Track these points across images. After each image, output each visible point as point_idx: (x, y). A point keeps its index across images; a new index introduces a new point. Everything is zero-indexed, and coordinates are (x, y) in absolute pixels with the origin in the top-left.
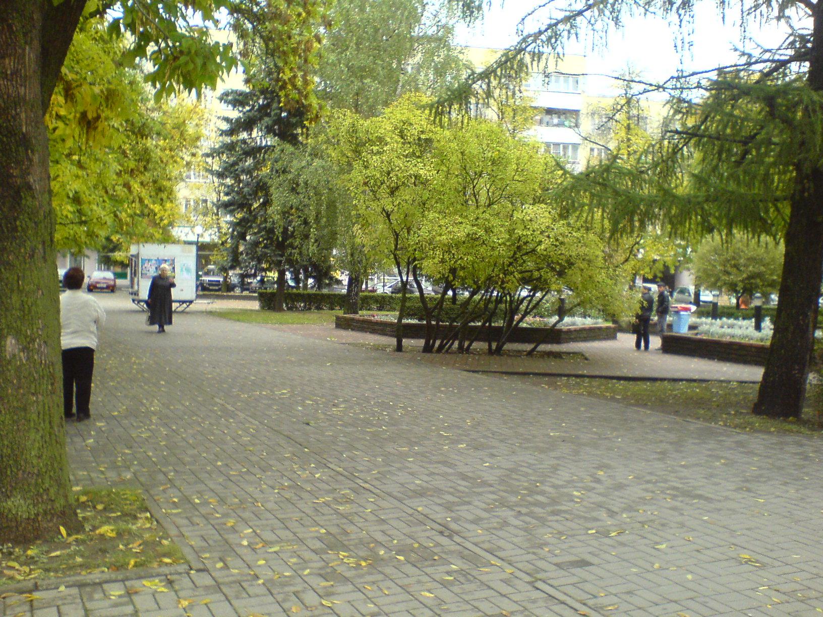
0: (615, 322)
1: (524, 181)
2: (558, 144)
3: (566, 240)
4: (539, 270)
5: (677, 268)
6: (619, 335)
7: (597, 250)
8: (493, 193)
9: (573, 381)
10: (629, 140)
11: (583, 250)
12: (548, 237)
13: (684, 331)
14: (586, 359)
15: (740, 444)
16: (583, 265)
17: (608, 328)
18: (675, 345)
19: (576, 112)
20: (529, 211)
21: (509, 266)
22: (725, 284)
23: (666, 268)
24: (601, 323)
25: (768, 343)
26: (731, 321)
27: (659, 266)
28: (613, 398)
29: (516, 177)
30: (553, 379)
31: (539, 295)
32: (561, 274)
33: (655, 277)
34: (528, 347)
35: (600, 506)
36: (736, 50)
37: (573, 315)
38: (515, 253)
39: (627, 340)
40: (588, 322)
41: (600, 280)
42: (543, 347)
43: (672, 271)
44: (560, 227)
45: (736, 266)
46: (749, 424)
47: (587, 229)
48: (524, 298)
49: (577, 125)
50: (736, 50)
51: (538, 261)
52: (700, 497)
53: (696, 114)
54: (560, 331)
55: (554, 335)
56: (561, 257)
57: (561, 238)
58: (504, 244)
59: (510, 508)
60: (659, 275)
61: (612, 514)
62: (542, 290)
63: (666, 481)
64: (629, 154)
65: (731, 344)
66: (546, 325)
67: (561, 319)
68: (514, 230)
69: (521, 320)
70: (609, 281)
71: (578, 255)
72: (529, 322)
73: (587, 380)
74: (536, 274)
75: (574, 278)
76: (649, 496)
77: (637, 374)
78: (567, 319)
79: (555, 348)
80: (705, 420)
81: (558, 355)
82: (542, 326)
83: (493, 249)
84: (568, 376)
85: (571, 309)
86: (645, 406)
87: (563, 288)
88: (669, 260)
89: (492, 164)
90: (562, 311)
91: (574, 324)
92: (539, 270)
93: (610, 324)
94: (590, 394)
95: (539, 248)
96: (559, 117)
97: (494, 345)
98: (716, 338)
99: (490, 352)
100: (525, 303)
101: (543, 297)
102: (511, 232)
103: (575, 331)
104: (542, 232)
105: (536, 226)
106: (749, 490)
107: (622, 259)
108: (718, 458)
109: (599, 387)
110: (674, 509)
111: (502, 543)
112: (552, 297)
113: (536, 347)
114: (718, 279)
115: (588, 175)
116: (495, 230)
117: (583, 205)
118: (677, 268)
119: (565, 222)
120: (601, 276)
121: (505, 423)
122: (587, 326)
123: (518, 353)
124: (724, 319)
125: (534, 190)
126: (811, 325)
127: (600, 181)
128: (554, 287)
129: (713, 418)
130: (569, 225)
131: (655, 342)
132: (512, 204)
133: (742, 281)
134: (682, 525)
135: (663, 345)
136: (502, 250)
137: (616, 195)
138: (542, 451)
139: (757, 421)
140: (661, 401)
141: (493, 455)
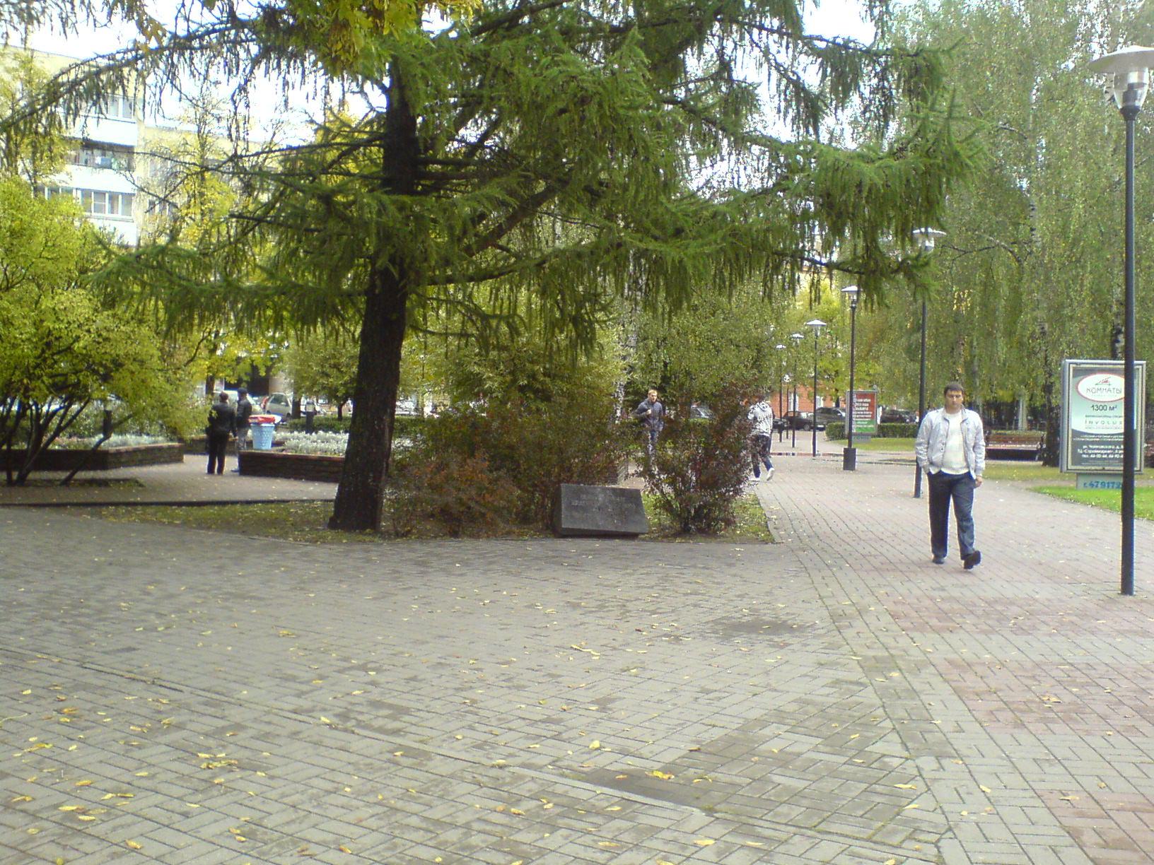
0: (180, 440)
1: (55, 260)
2: (103, 193)
3: (111, 336)
4: (76, 372)
5: (268, 369)
6: (185, 457)
7: (151, 347)
8: (13, 274)
9: (122, 510)
10: (202, 194)
11: (132, 349)
12: (89, 331)
13: (267, 447)
14: (141, 485)
15: (306, 554)
16: (135, 367)
17: (170, 448)
18: (255, 465)
19: (129, 150)
20: (63, 298)
21: (35, 368)
22: (324, 388)
23: (255, 369)
24: (162, 442)
25: (342, 456)
26: (330, 434)
27: (244, 367)
28: (170, 523)
29: (45, 254)
30: (98, 509)
31: (75, 407)
32: (106, 378)
33: (240, 381)
34: (63, 475)
35: (150, 611)
36: (312, 122)
37: (122, 433)
38: (43, 351)
39: (198, 463)
40: (145, 441)
41: (156, 385)
42: (82, 475)
43: (263, 373)
44: (104, 319)
45: (336, 366)
46: (321, 537)
47: (141, 322)
48: (55, 412)
49: (130, 168)
50: (312, 122)
51: (75, 361)
52: (251, 598)
53: (268, 190)
54: (106, 453)
55: (99, 459)
56: (107, 357)
57: (104, 334)
58: (29, 339)
59: (54, 620)
60: (245, 378)
61: (160, 615)
62: (80, 399)
63: (220, 588)
64: (203, 214)
65: (321, 460)
66: (86, 446)
67: (107, 437)
68: (42, 321)
69: (51, 440)
70: (168, 387)
71: (127, 355)
72: (63, 442)
73: (140, 508)
74: (73, 379)
75: (122, 384)
76: (199, 601)
77: (204, 498)
78: (114, 438)
79: (100, 474)
80: (273, 537)
81: (104, 483)
82: (82, 448)
83: (14, 346)
84: (117, 504)
85: (120, 423)
86: (209, 528)
87: (111, 397)
88: (258, 358)
89: (12, 235)
90: (108, 425)
91: (124, 444)
92: (76, 372)
93: (176, 444)
94: (143, 521)
95: (76, 346)
96: (104, 155)
97: (15, 475)
98: (304, 453)
99: (10, 482)
100: (56, 420)
101: (82, 408)
102: (38, 324)
103: (127, 452)
104: (80, 326)
105: (71, 318)
106: (302, 589)
107: (185, 358)
108: (278, 567)
109: (155, 514)
110: (226, 608)
111: (46, 644)
112: (95, 407)
113: (73, 474)
114: (314, 385)
115: (138, 257)
116: (16, 323)
117: (133, 294)
118: (268, 369)
119: (110, 312)
120: (158, 381)
121: (39, 553)
122: (141, 446)
123: (50, 482)
124: (321, 432)
125: (69, 271)
126: (387, 430)
127: (151, 264)
128: (96, 395)
129: (285, 535)
130: (114, 316)
131: (232, 463)
132: (39, 286)
133: (345, 384)
134: (230, 618)
135: (240, 465)
136: (26, 349)
137: (173, 285)
138: (85, 574)
139: (330, 534)
140: (228, 523)
141: (27, 582)
